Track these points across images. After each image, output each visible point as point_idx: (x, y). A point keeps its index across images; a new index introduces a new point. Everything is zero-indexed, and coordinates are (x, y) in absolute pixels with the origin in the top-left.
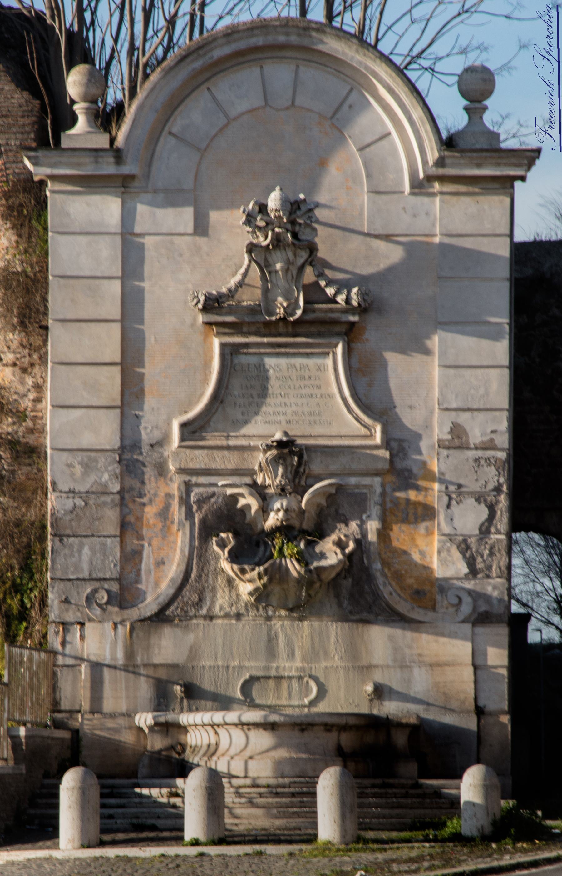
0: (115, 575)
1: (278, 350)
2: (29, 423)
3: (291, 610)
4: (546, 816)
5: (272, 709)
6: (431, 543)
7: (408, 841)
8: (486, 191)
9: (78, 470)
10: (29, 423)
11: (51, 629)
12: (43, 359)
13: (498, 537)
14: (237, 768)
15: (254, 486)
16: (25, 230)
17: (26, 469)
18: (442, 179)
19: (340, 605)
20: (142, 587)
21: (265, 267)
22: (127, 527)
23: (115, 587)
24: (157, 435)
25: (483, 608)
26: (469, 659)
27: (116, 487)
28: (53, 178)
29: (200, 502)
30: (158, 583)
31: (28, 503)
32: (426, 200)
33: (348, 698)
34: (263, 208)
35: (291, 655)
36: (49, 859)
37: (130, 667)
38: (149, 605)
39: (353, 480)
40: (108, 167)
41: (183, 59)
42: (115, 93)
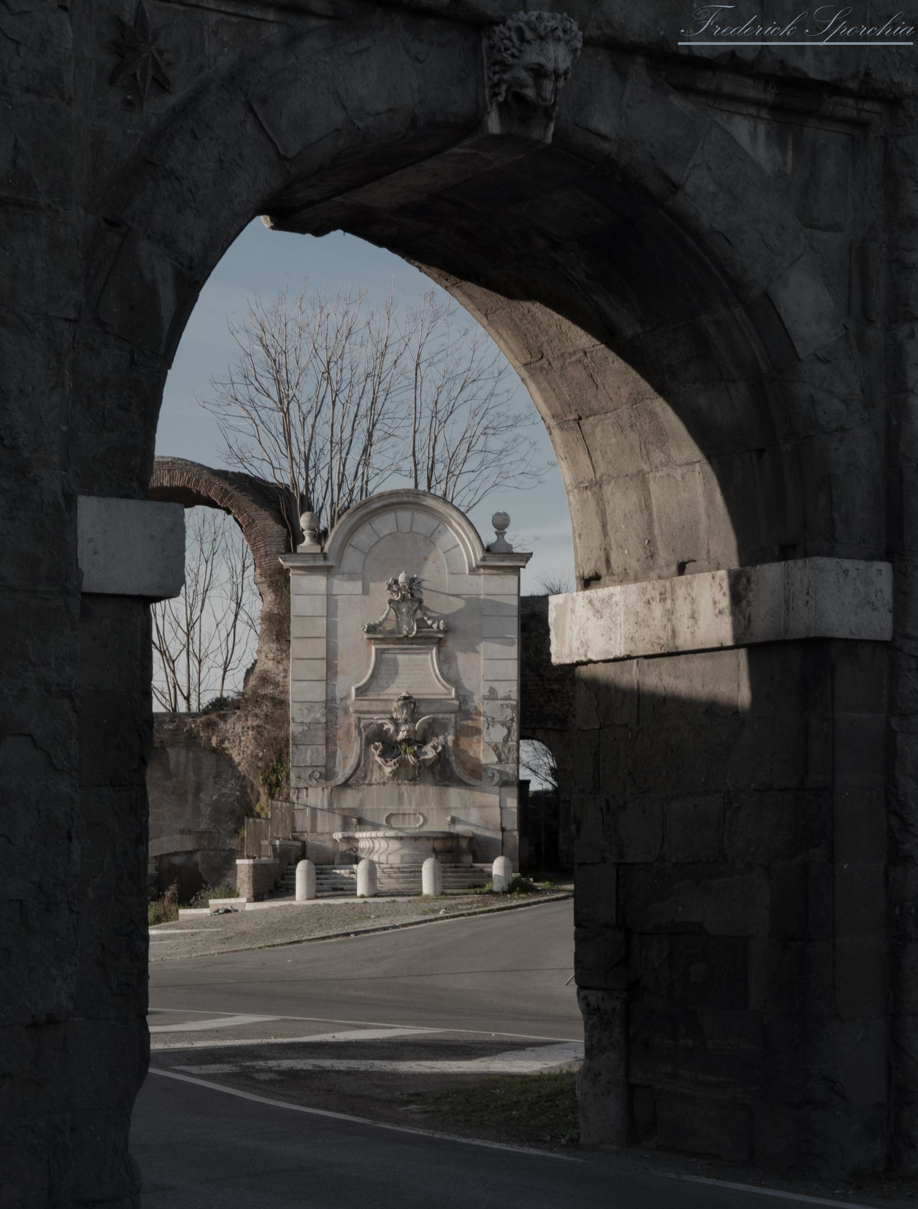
0: (323, 764)
1: (404, 651)
2: (281, 688)
3: (410, 780)
4: (535, 881)
5: (400, 829)
6: (479, 747)
7: (467, 894)
8: (505, 573)
9: (305, 711)
10: (281, 688)
11: (292, 791)
12: (288, 656)
13: (512, 743)
14: (383, 859)
15: (392, 719)
16: (279, 593)
17: (279, 711)
18: (484, 567)
19: (434, 778)
20: (336, 770)
21: (397, 611)
22: (329, 741)
23: (323, 770)
24: (344, 694)
25: (505, 778)
26: (498, 804)
27: (324, 720)
28: (293, 567)
29: (365, 727)
30: (343, 772)
31: (280, 728)
32: (476, 577)
33: (438, 824)
34: (396, 582)
35: (410, 803)
36: (291, 906)
37: (331, 810)
38: (340, 779)
39: (441, 716)
40: (320, 563)
41: (357, 509)
42: (324, 523)
